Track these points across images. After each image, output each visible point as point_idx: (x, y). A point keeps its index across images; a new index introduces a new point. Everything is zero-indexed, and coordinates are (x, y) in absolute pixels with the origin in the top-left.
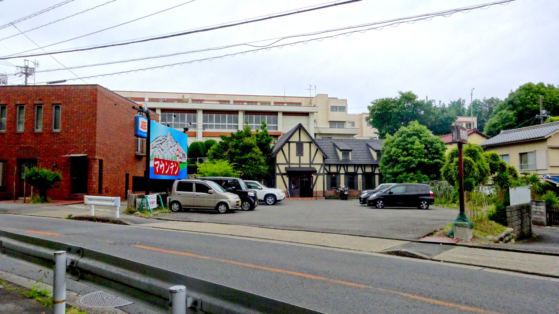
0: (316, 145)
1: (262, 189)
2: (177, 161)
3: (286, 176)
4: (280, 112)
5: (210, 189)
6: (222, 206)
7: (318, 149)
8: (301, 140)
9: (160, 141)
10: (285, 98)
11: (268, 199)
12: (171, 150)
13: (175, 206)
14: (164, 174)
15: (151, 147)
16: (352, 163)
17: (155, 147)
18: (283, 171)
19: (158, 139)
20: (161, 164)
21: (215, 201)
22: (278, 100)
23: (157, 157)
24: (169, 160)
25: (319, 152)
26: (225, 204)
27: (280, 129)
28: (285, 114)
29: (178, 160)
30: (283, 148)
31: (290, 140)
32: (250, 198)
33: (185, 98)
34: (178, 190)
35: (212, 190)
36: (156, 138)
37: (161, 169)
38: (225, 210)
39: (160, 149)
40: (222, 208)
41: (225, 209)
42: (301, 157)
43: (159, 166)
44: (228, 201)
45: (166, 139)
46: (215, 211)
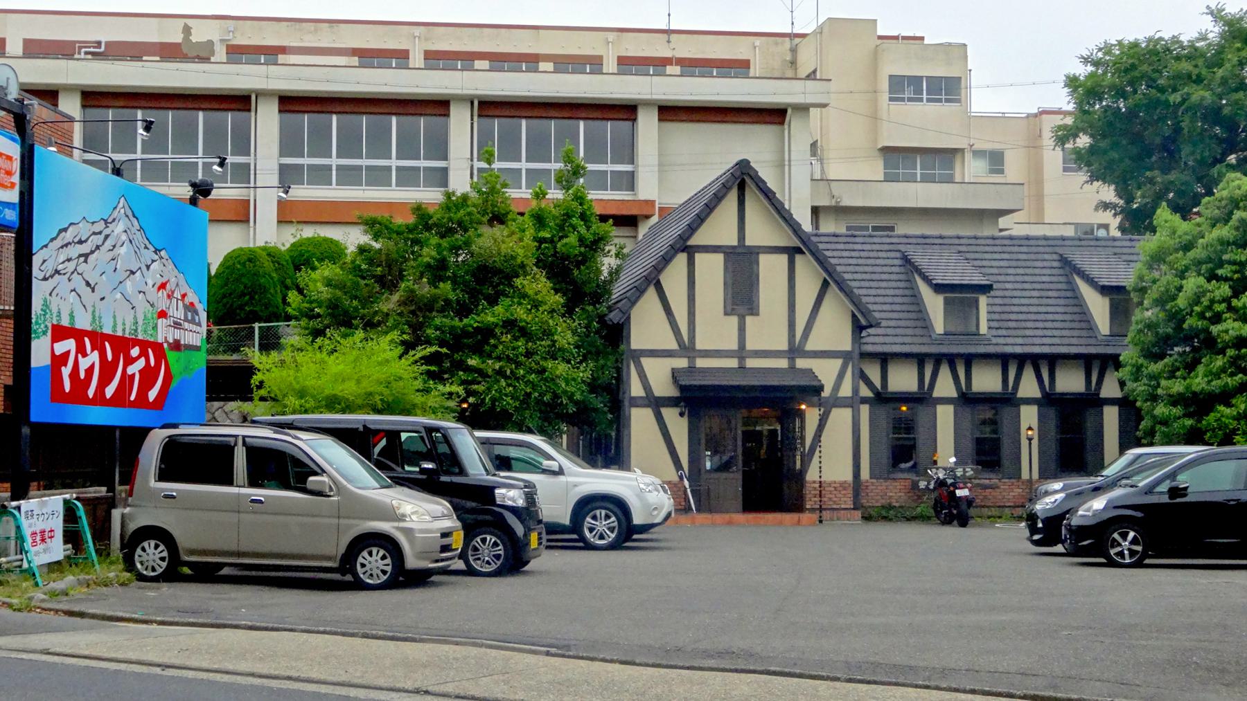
0: (822, 261)
1: (560, 472)
2: (160, 341)
3: (676, 411)
4: (648, 103)
6: (370, 554)
7: (831, 280)
9: (81, 242)
10: (674, 37)
11: (588, 519)
14: (100, 399)
18: (663, 387)
19: (68, 236)
20: (85, 355)
23: (65, 322)
24: (120, 333)
26: (388, 544)
27: (648, 189)
28: (669, 112)
30: (665, 279)
31: (693, 241)
33: (194, 39)
34: (163, 476)
35: (324, 478)
37: (82, 375)
38: (384, 572)
39: (78, 281)
42: (749, 319)
44: (398, 528)
45: (107, 237)
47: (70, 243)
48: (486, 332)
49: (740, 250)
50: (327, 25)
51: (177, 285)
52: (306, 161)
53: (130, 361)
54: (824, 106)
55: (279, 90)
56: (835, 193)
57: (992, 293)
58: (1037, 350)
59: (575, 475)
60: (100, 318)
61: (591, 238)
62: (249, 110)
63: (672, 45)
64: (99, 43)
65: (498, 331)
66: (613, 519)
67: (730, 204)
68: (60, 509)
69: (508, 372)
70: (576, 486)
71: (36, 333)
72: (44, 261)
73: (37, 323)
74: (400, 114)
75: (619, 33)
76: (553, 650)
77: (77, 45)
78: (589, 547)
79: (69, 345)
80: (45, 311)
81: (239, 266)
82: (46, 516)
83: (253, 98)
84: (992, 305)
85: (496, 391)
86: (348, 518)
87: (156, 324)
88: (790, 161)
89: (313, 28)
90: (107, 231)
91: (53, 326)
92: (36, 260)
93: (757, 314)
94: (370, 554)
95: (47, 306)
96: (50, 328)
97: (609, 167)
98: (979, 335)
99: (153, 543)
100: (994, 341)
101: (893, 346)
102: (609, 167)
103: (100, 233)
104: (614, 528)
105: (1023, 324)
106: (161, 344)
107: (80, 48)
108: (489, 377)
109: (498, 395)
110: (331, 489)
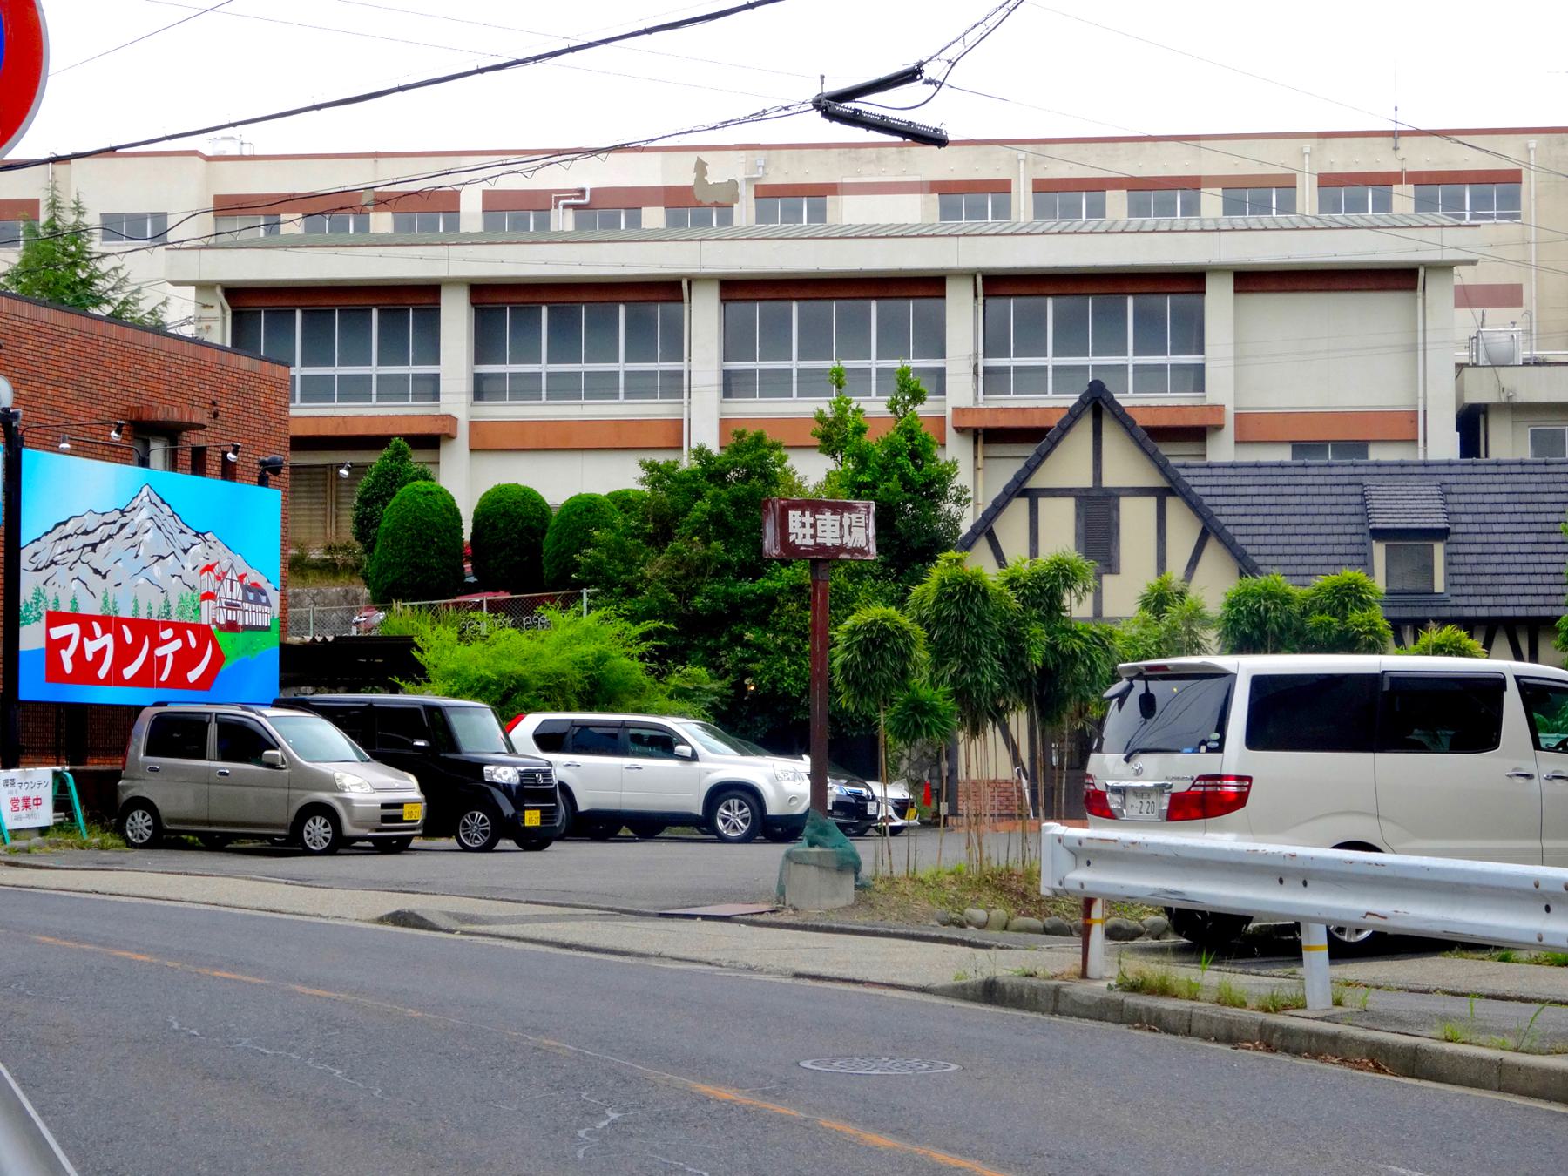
0: (1195, 506)
1: (694, 757)
2: (205, 622)
4: (1219, 270)
5: (273, 748)
6: (314, 822)
7: (1210, 530)
8: (1109, 481)
9: (86, 533)
10: (1404, 142)
11: (722, 809)
12: (157, 571)
13: (139, 823)
14: (115, 678)
15: (25, 563)
16: (1456, 612)
17: (53, 562)
19: (69, 528)
20: (93, 637)
21: (289, 801)
22: (1343, 160)
23: (66, 608)
24: (143, 616)
25: (1212, 551)
26: (327, 812)
27: (1221, 390)
28: (1250, 280)
29: (209, 614)
30: (999, 527)
31: (1034, 482)
32: (494, 791)
33: (710, 179)
34: (149, 752)
35: (279, 753)
36: (58, 525)
37: (89, 657)
38: (326, 839)
39: (83, 571)
40: (317, 830)
41: (329, 836)
42: (1107, 579)
43: (81, 647)
44: (339, 799)
45: (123, 526)
46: (288, 843)
47: (71, 535)
48: (770, 599)
49: (1094, 494)
50: (894, 149)
51: (232, 566)
52: (758, 365)
53: (157, 643)
54: (1473, 263)
55: (719, 274)
56: (1506, 383)
57: (1452, 538)
58: (1508, 612)
59: (712, 761)
60: (115, 603)
61: (922, 481)
62: (682, 301)
63: (1401, 154)
64: (582, 191)
65: (780, 599)
66: (746, 809)
67: (1084, 430)
68: (50, 778)
69: (793, 648)
70: (708, 773)
71: (24, 619)
72: (36, 554)
73: (26, 611)
74: (883, 298)
75: (1321, 140)
76: (290, 881)
77: (554, 196)
78: (724, 840)
79: (73, 629)
80: (37, 599)
81: (574, 518)
82: (31, 785)
83: (685, 284)
84: (1452, 554)
85: (777, 669)
86: (297, 788)
87: (199, 608)
88: (1424, 343)
89: (874, 156)
90: (124, 520)
91: (49, 613)
92: (25, 555)
93: (1118, 573)
94: (314, 822)
95: (40, 594)
96: (45, 615)
97: (1169, 359)
98: (1433, 593)
99: (141, 813)
100: (1453, 601)
101: (1479, 609)
102: (1169, 359)
103: (114, 522)
104: (748, 819)
105: (1500, 579)
106: (209, 626)
107: (557, 199)
108: (771, 653)
109: (779, 675)
110: (283, 762)
